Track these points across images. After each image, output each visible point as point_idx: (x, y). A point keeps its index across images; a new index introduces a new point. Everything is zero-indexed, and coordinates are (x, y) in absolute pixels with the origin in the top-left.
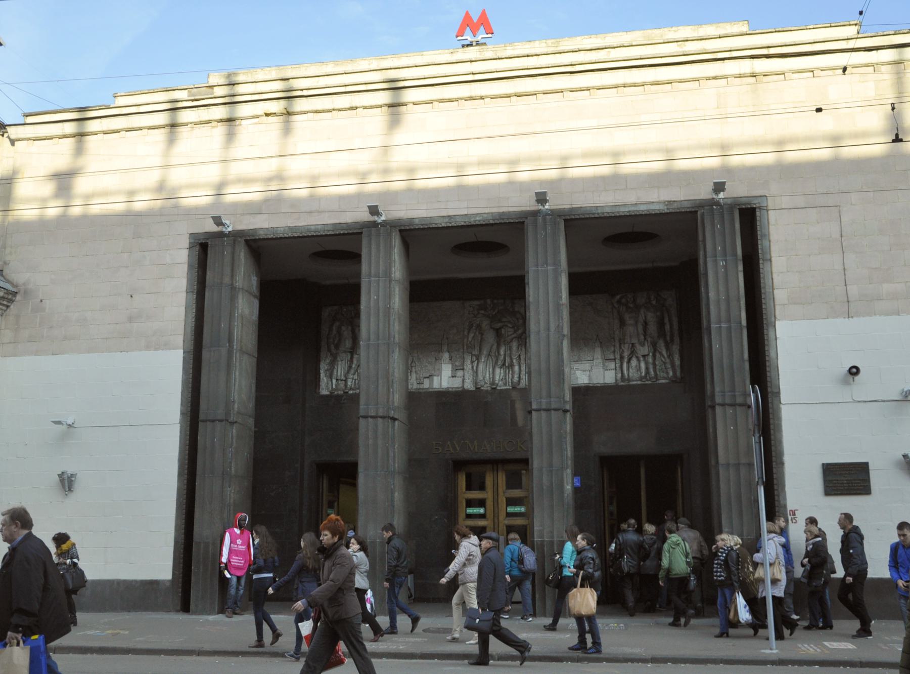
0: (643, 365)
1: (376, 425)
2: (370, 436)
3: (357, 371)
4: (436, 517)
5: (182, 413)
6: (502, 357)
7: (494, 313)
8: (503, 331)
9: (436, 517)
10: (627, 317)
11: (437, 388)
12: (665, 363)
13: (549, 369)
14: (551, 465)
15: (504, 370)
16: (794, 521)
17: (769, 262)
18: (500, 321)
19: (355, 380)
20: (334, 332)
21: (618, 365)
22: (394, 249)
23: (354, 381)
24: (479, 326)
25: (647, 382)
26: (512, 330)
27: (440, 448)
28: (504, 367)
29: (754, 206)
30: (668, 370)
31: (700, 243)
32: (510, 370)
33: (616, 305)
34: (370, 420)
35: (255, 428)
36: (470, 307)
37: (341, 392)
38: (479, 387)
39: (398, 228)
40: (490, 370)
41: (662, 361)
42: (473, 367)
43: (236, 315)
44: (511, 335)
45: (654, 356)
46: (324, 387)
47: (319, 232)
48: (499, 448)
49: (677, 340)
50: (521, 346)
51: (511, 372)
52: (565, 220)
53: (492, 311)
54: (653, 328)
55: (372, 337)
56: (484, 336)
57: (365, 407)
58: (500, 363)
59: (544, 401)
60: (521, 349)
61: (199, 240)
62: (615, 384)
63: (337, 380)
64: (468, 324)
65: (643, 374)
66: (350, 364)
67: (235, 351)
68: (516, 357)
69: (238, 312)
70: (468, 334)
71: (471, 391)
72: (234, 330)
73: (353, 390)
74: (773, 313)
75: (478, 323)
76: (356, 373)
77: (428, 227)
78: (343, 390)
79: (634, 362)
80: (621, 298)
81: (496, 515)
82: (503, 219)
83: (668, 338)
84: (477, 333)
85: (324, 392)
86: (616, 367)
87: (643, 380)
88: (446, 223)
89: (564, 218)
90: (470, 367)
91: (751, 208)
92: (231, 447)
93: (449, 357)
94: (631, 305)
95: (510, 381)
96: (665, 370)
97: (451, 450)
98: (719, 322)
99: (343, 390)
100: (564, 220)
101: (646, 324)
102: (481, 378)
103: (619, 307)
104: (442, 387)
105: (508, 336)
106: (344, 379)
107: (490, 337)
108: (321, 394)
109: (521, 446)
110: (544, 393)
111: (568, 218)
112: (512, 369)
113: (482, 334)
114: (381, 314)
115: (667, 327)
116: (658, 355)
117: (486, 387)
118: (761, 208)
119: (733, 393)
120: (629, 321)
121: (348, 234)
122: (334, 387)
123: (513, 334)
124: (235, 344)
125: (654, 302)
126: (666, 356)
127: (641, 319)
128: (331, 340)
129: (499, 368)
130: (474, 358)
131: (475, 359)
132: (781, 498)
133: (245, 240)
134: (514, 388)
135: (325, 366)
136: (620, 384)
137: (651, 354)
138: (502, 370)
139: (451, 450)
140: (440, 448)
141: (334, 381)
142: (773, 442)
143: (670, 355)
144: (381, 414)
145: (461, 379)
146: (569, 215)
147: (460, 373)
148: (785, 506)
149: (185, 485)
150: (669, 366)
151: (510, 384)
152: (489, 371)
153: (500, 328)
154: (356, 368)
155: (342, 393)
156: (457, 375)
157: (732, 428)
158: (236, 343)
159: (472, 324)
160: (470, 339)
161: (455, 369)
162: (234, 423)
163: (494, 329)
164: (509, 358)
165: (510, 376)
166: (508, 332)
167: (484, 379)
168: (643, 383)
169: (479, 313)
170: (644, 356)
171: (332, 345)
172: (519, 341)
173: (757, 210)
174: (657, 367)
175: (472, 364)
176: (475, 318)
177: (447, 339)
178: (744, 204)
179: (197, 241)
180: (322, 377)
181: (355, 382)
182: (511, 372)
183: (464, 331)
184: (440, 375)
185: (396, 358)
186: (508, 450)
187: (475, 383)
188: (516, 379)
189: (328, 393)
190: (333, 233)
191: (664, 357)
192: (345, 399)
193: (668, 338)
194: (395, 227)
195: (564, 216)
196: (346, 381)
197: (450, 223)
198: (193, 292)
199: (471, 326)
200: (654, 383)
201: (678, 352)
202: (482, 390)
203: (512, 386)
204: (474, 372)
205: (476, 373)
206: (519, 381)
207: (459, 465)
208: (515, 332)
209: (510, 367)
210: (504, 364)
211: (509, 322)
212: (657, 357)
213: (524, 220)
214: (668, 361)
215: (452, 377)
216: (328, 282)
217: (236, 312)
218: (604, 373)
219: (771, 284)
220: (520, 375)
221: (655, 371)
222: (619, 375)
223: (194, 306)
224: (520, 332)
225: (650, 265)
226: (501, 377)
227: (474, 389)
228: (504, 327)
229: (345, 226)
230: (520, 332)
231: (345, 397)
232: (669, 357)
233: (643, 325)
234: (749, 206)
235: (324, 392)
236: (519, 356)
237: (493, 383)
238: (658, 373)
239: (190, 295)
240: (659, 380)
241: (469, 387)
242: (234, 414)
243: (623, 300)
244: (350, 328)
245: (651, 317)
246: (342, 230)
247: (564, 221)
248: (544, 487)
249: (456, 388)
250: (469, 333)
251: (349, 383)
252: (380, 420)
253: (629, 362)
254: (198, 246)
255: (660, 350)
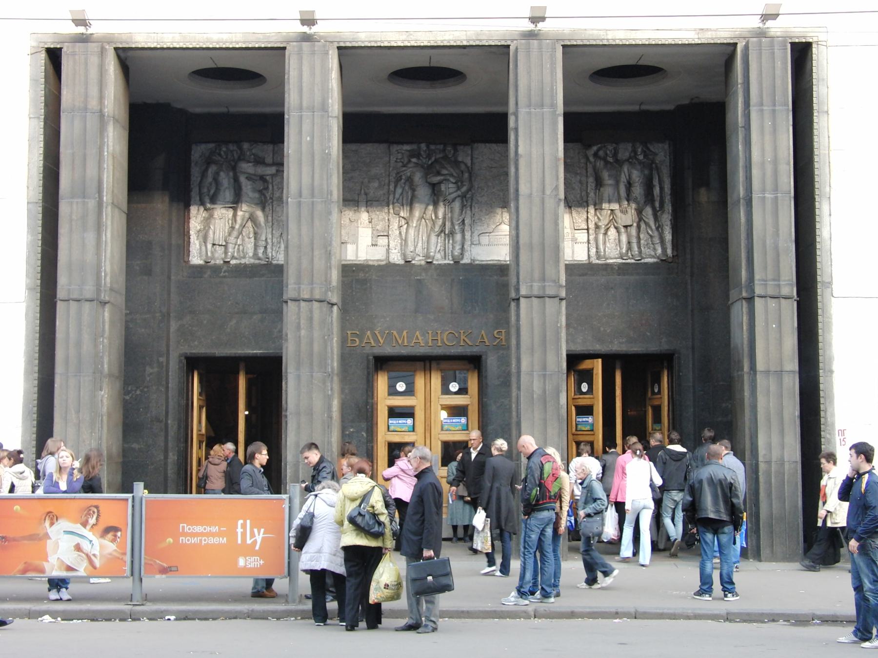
0: (624, 238)
1: (311, 311)
2: (302, 326)
3: (240, 233)
4: (351, 430)
5: (30, 289)
6: (441, 220)
7: (430, 162)
8: (443, 187)
9: (351, 430)
10: (605, 175)
11: (352, 260)
12: (651, 236)
13: (543, 244)
14: (544, 367)
15: (443, 239)
16: (843, 443)
17: (826, 116)
18: (439, 173)
19: (239, 245)
20: (210, 179)
21: (592, 237)
22: (332, 73)
23: (237, 246)
24: (410, 180)
25: (629, 261)
26: (454, 186)
27: (357, 340)
28: (443, 235)
29: (811, 40)
30: (656, 245)
31: (739, 86)
32: (451, 239)
33: (592, 159)
34: (303, 304)
35: (125, 309)
36: (398, 153)
37: (219, 262)
38: (410, 260)
39: (336, 45)
40: (424, 238)
41: (648, 233)
42: (400, 233)
43: (106, 153)
44: (452, 193)
45: (639, 227)
46: (196, 254)
47: (225, 43)
48: (436, 341)
49: (668, 207)
50: (466, 208)
51: (451, 241)
52: (564, 46)
53: (427, 159)
54: (638, 190)
55: (305, 192)
56: (416, 193)
57: (296, 286)
58: (437, 229)
59: (536, 285)
60: (466, 213)
61: (45, 43)
62: (587, 262)
63: (214, 245)
64: (394, 175)
65: (624, 251)
66: (232, 224)
67: (104, 204)
68: (459, 222)
69: (108, 149)
70: (395, 189)
71: (399, 264)
72: (103, 175)
73: (236, 259)
74: (828, 181)
75: (409, 174)
76: (240, 237)
77: (379, 45)
78: (223, 259)
79: (612, 232)
80: (598, 150)
81: (428, 428)
82: (480, 40)
83: (657, 204)
84: (407, 188)
85: (196, 259)
86: (588, 240)
87: (625, 258)
88: (403, 41)
89: (563, 43)
90: (398, 232)
91: (806, 42)
92: (102, 336)
93: (369, 219)
94: (610, 160)
95: (450, 254)
96: (652, 245)
97: (372, 341)
98: (764, 191)
99: (223, 259)
100: (562, 45)
101: (629, 185)
102: (412, 249)
103: (595, 162)
104: (359, 259)
105: (449, 194)
106: (224, 243)
107: (423, 191)
108: (192, 263)
109: (466, 339)
110: (537, 275)
111: (569, 43)
112: (453, 236)
113: (414, 190)
114: (316, 162)
115: (657, 191)
116: (643, 226)
117: (419, 261)
118: (819, 43)
119: (776, 283)
120: (608, 181)
121: (266, 48)
122: (209, 254)
123: (456, 191)
124: (105, 194)
125: (641, 157)
126: (654, 227)
127: (623, 179)
128: (205, 190)
129: (436, 235)
130: (403, 222)
131: (403, 224)
132: (828, 414)
133: (114, 48)
134: (457, 263)
135: (197, 224)
136: (594, 262)
137: (635, 224)
138: (439, 238)
139: (372, 341)
140: (357, 340)
141: (209, 246)
142: (820, 345)
143: (659, 228)
144: (317, 297)
145: (384, 249)
146: (569, 40)
147: (383, 241)
148: (833, 424)
149: (35, 387)
150: (657, 240)
151: (450, 257)
152: (422, 240)
153: (440, 183)
154: (240, 229)
155: (222, 262)
156: (379, 244)
157: (774, 326)
158: (107, 192)
159: (401, 176)
160: (397, 196)
161: (377, 235)
162: (106, 303)
163: (430, 184)
164: (450, 224)
165: (451, 247)
166: (448, 188)
167: (415, 250)
168: (624, 261)
169: (410, 161)
170: (626, 227)
171: (207, 197)
172: (462, 201)
173: (814, 46)
174: (642, 242)
175: (400, 229)
176: (404, 169)
177: (366, 194)
178: (798, 37)
179: (42, 45)
180: (192, 240)
181: (238, 249)
182: (451, 241)
183: (389, 185)
184: (355, 242)
185: (335, 221)
186: (446, 343)
187: (404, 255)
188: (457, 252)
189: (201, 262)
190: (244, 46)
191: (652, 230)
192: (225, 272)
193: (657, 204)
194: (332, 42)
195: (563, 40)
196: (226, 246)
197: (409, 41)
198: (38, 118)
199: (398, 180)
200: (640, 262)
201: (669, 223)
202: (413, 264)
203: (453, 260)
204: (402, 239)
205: (404, 242)
206: (462, 254)
207: (382, 362)
208: (459, 189)
209: (451, 235)
210: (442, 231)
211: (452, 175)
212: (642, 228)
213: (509, 43)
214: (656, 234)
215: (373, 245)
216: (198, 110)
217: (106, 150)
218: (573, 246)
219: (827, 144)
220: (463, 246)
221: (639, 247)
222: (593, 251)
223: (42, 138)
224: (464, 189)
225: (636, 108)
226: (438, 248)
227: (403, 263)
228: (444, 182)
229: (261, 37)
230: (464, 189)
231: (225, 268)
232: (657, 229)
233: (626, 186)
234: (804, 41)
235: (196, 259)
236: (463, 220)
237: (427, 256)
238: (643, 249)
239: (35, 121)
240: (644, 258)
241: (396, 259)
242: (105, 291)
243: (601, 153)
244: (231, 174)
245: (636, 175)
246: (257, 42)
247: (563, 48)
248: (535, 396)
249: (378, 260)
250: (395, 187)
251: (230, 250)
252: (316, 305)
253: (605, 234)
254: (44, 52)
255: (646, 220)
